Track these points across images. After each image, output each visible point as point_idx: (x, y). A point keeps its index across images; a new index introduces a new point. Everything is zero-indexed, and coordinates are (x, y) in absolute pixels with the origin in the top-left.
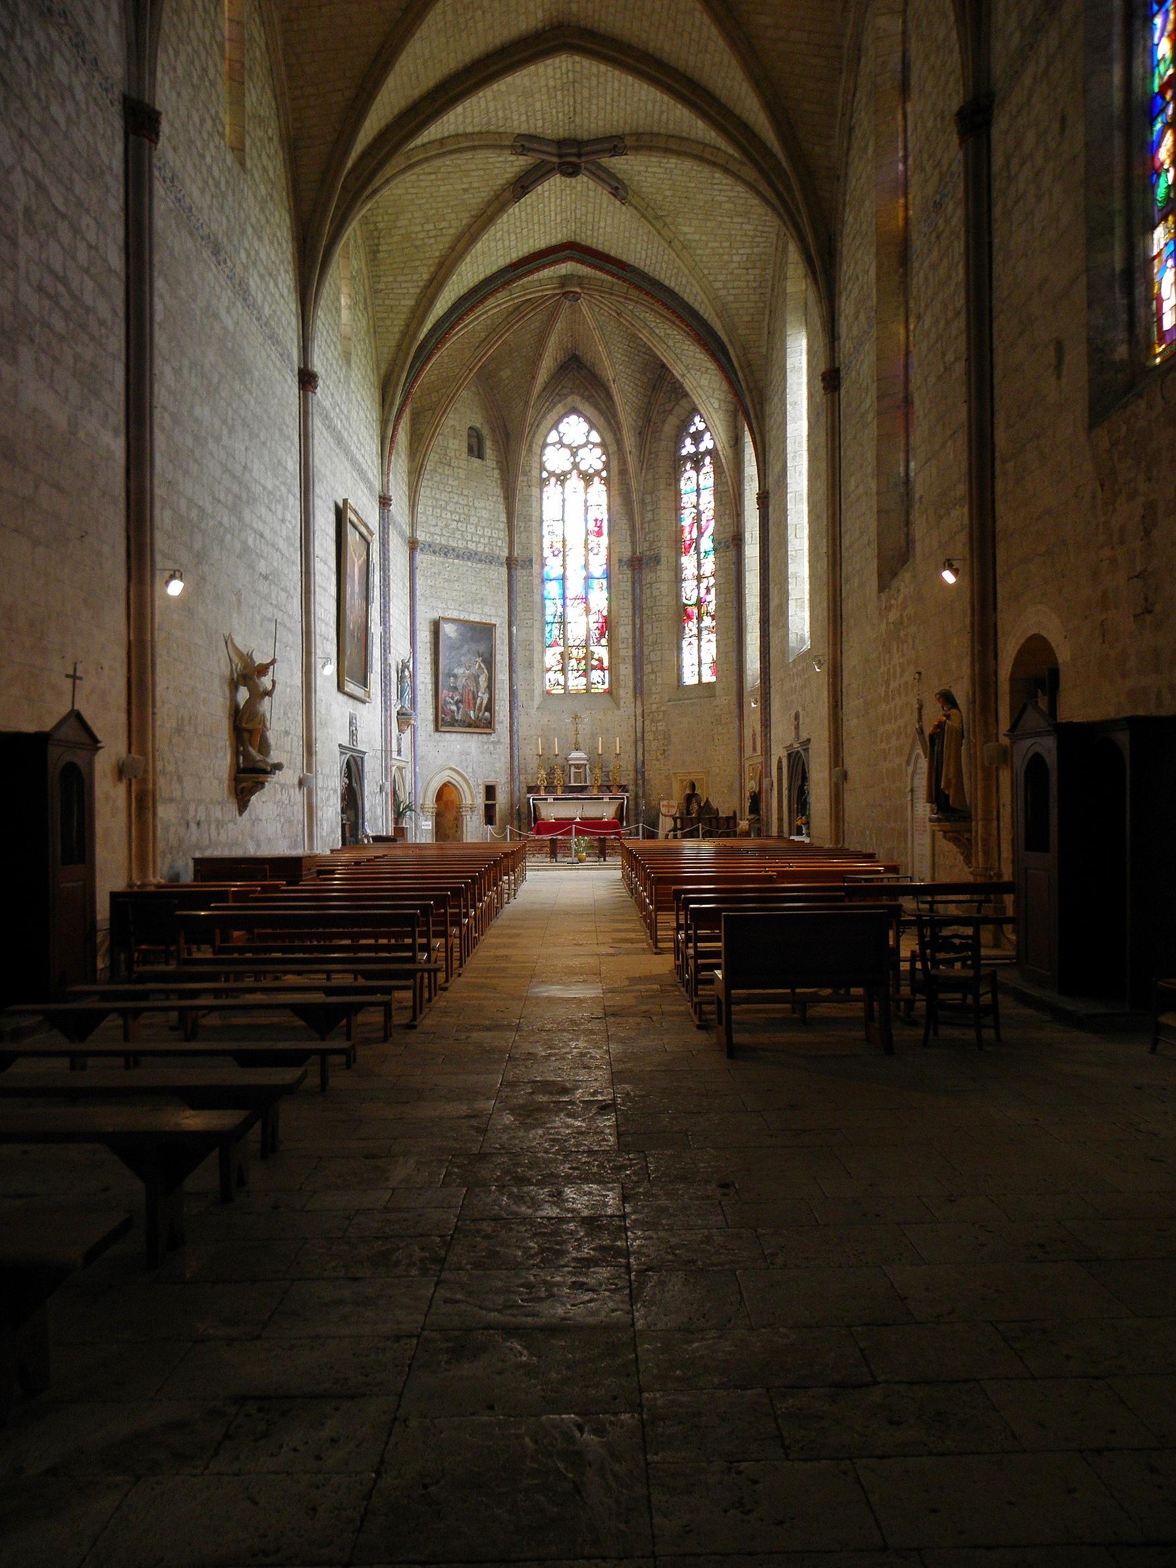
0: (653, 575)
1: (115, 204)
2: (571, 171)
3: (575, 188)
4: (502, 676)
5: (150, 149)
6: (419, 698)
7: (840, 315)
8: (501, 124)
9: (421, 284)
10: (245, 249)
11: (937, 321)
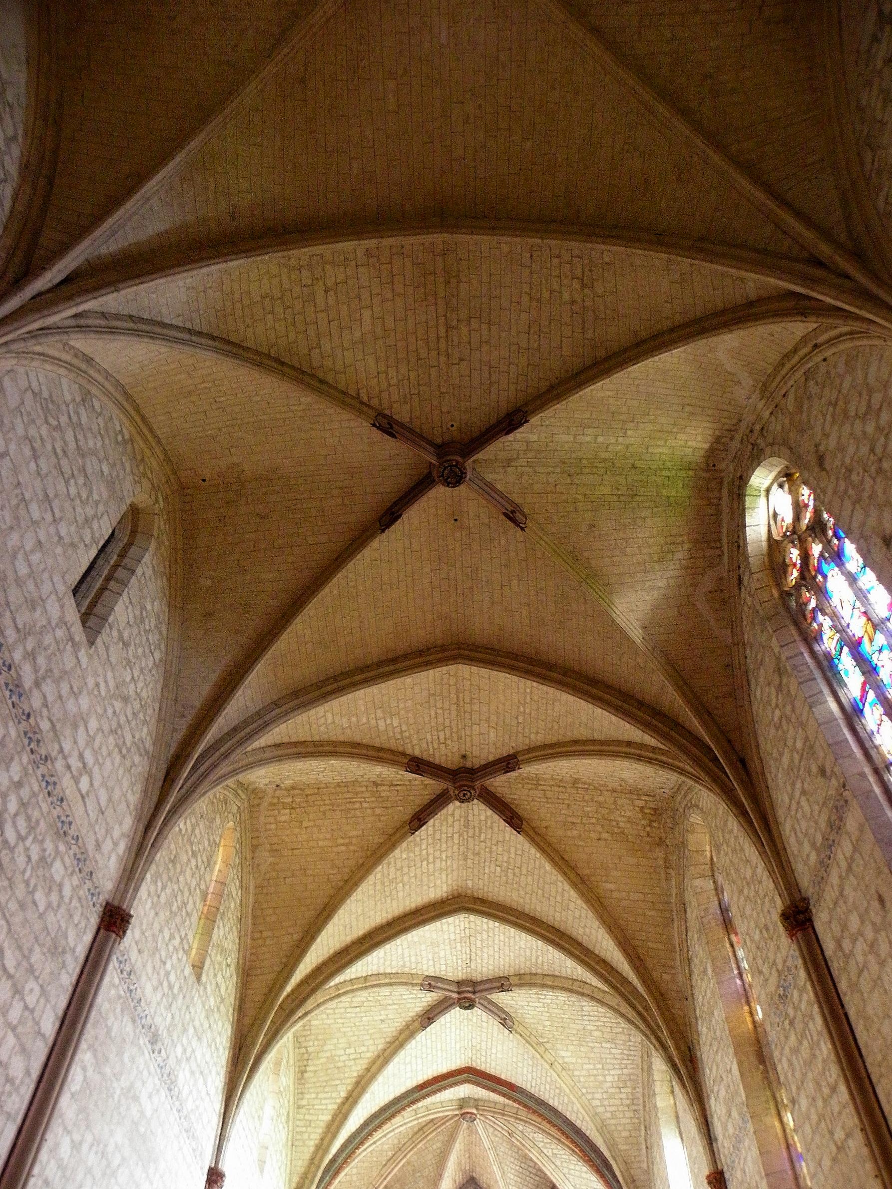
1: (68, 979)
2: (469, 1005)
3: (471, 1020)
5: (115, 941)
9: (339, 1101)
10: (183, 1046)
11: (814, 1099)
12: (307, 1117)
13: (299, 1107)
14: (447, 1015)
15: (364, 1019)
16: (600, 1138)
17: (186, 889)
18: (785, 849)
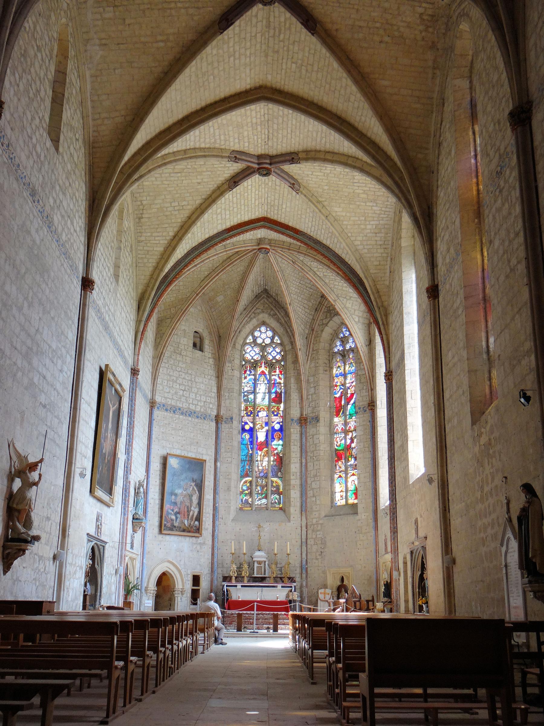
0: (314, 430)
2: (267, 173)
3: (268, 184)
4: (208, 496)
6: (149, 509)
7: (437, 253)
8: (222, 143)
9: (168, 238)
10: (53, 198)
11: (503, 241)
12: (145, 248)
13: (139, 242)
14: (249, 180)
15: (184, 182)
16: (357, 265)
17: (37, 78)
18: (525, 60)
